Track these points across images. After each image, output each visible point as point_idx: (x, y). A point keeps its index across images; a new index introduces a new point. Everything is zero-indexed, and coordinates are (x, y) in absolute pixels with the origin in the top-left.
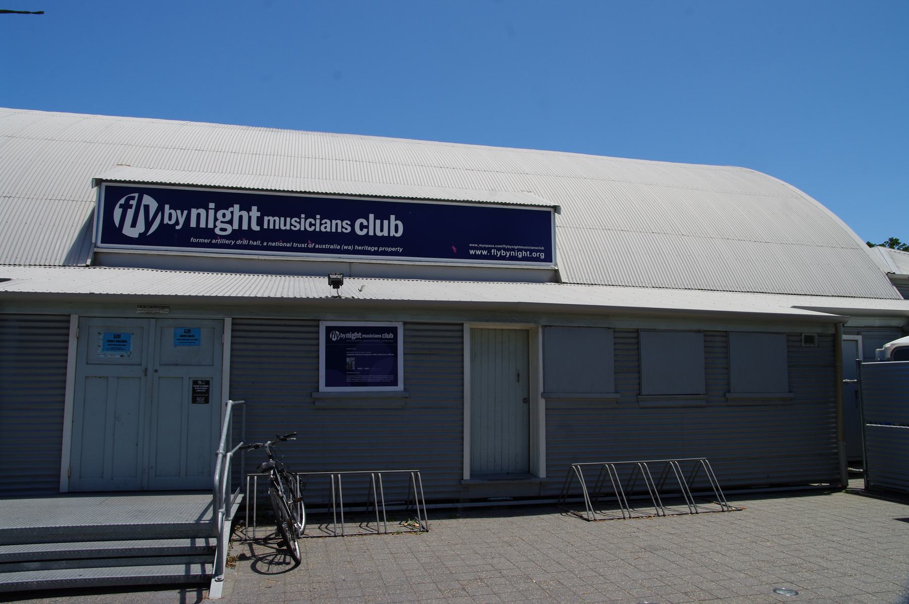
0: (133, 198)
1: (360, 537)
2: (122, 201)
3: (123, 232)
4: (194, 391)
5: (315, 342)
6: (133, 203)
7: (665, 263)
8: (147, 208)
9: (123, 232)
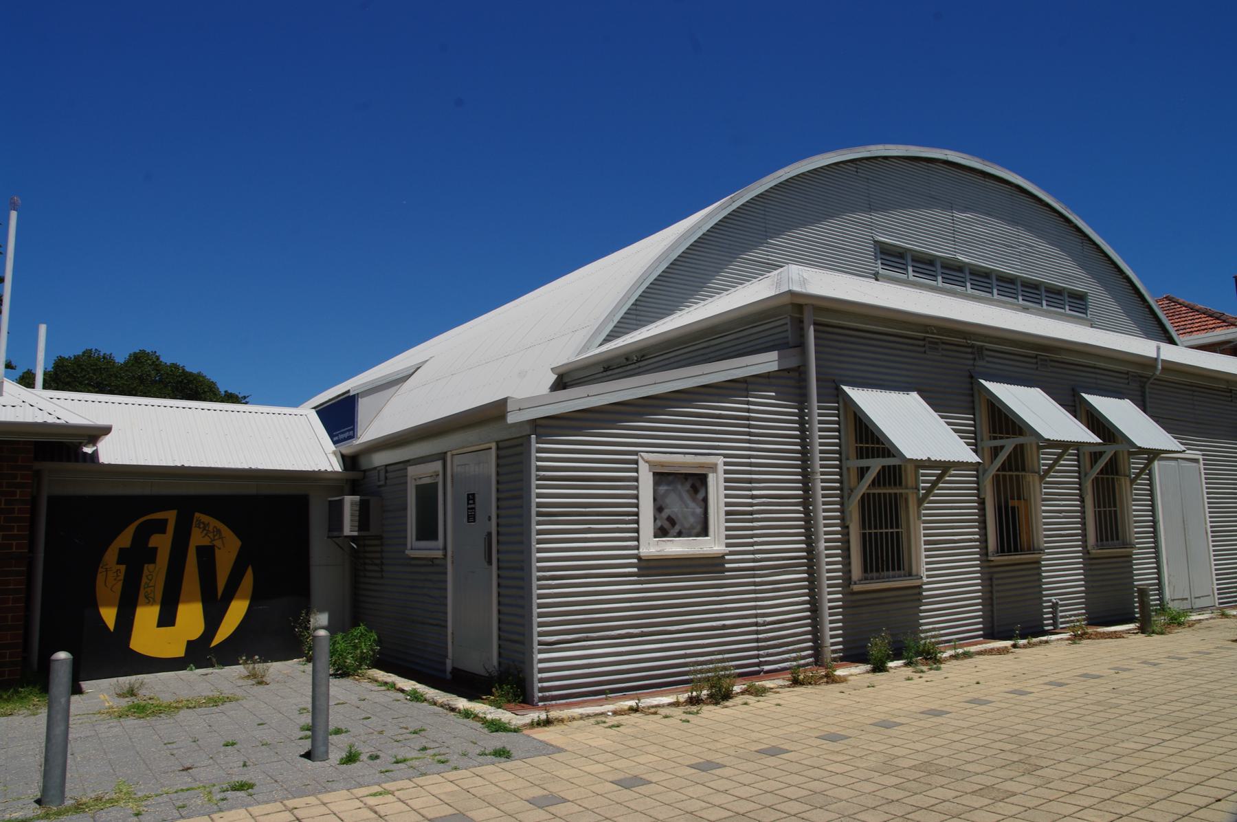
0: (161, 526)
1: (170, 741)
2: (125, 539)
3: (183, 655)
4: (468, 515)
5: (503, 453)
6: (162, 543)
7: (778, 214)
8: (207, 556)
9: (183, 655)
